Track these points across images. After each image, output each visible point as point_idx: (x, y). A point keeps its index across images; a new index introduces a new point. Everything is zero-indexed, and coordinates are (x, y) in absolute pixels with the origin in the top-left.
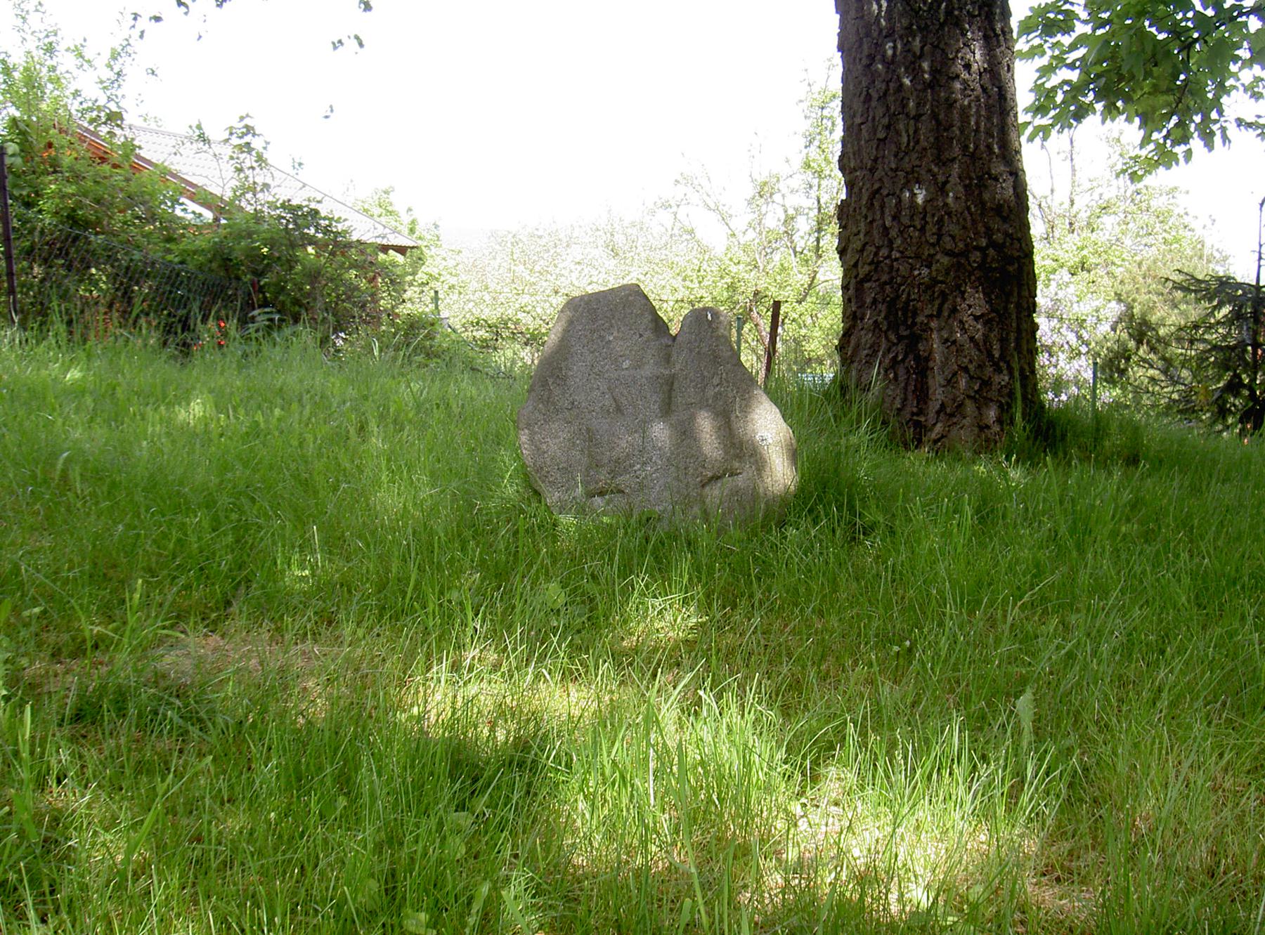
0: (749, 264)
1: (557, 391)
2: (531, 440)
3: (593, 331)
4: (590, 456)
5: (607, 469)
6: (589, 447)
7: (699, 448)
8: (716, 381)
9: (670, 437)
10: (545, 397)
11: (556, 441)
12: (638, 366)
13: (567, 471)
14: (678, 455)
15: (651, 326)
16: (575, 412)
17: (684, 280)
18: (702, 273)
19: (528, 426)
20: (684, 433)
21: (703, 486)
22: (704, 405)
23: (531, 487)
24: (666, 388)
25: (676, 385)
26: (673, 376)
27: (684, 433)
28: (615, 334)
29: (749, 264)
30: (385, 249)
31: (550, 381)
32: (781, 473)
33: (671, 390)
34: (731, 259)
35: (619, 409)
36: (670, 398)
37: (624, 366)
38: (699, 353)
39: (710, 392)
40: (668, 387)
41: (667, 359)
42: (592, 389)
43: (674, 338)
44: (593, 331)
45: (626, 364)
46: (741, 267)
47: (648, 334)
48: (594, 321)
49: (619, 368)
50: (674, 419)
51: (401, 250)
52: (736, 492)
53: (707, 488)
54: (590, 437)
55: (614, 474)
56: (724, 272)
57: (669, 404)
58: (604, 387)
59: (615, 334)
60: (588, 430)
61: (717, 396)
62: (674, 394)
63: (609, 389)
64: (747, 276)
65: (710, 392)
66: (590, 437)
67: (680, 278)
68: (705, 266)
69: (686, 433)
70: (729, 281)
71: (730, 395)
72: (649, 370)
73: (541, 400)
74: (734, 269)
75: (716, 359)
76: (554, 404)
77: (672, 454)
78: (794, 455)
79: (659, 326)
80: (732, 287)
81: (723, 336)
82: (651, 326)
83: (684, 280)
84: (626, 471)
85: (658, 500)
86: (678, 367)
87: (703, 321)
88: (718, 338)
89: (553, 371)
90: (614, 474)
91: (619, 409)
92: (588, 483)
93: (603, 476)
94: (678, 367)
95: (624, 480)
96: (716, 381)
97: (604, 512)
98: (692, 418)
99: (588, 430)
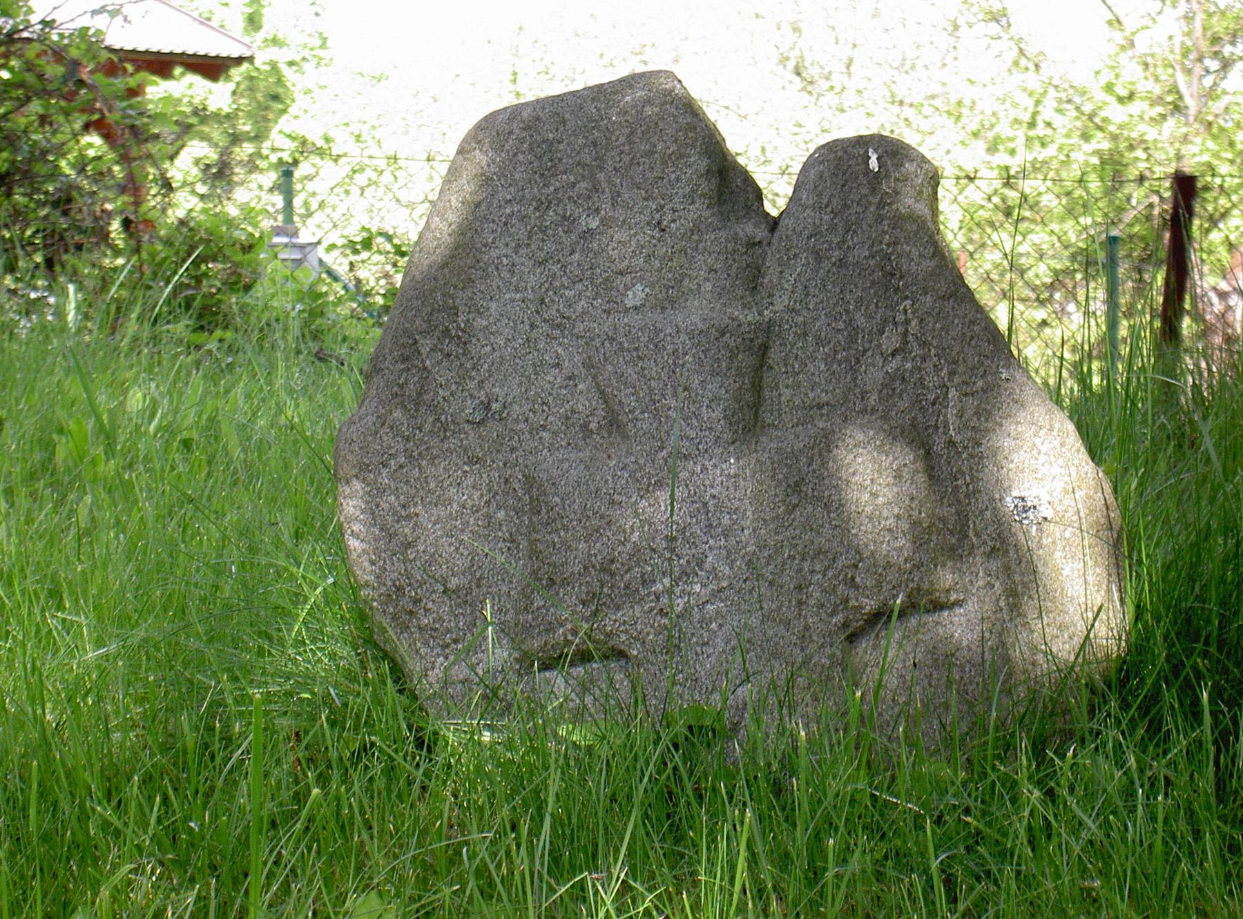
0: (1159, 100)
1: (444, 375)
2: (373, 511)
3: (543, 205)
4: (534, 553)
5: (582, 590)
6: (532, 529)
7: (843, 527)
8: (890, 341)
9: (757, 498)
10: (411, 390)
11: (454, 520)
12: (669, 300)
13: (465, 599)
14: (778, 548)
15: (704, 187)
16: (494, 428)
17: (992, 149)
18: (1040, 130)
19: (363, 469)
20: (797, 487)
21: (852, 638)
22: (851, 406)
23: (369, 641)
24: (746, 361)
25: (775, 355)
26: (768, 329)
27: (797, 487)
28: (606, 209)
29: (1159, 100)
30: (161, 64)
31: (426, 344)
32: (1082, 600)
33: (761, 366)
34: (1109, 88)
35: (614, 423)
36: (757, 388)
37: (630, 301)
38: (842, 263)
39: (873, 374)
40: (754, 358)
41: (752, 280)
42: (539, 367)
43: (774, 224)
44: (543, 205)
45: (636, 295)
46: (1137, 107)
47: (699, 210)
48: (547, 174)
49: (614, 306)
50: (769, 444)
51: (212, 67)
52: (943, 659)
53: (864, 644)
54: (533, 500)
55: (596, 603)
56: (1092, 124)
57: (756, 406)
58: (572, 359)
59: (606, 209)
60: (529, 482)
61: (889, 387)
62: (768, 379)
63: (588, 365)
64: (1151, 134)
65: (873, 374)
66: (533, 500)
67: (980, 146)
68: (1047, 113)
69: (806, 486)
70: (1106, 145)
71: (931, 381)
72: (697, 312)
73: (398, 397)
74: (1116, 114)
75: (889, 280)
76: (434, 408)
77: (762, 547)
78: (1121, 545)
79: (729, 184)
80: (1113, 169)
81: (913, 217)
82: (704, 187)
83: (992, 149)
84: (630, 593)
85: (718, 671)
86: (781, 302)
87: (866, 181)
88: (898, 221)
89: (435, 309)
90: (596, 603)
91: (614, 423)
92: (527, 629)
93: (568, 618)
94: (781, 302)
95: (628, 621)
96: (890, 341)
97: (572, 719)
98: (825, 444)
99: (529, 482)
